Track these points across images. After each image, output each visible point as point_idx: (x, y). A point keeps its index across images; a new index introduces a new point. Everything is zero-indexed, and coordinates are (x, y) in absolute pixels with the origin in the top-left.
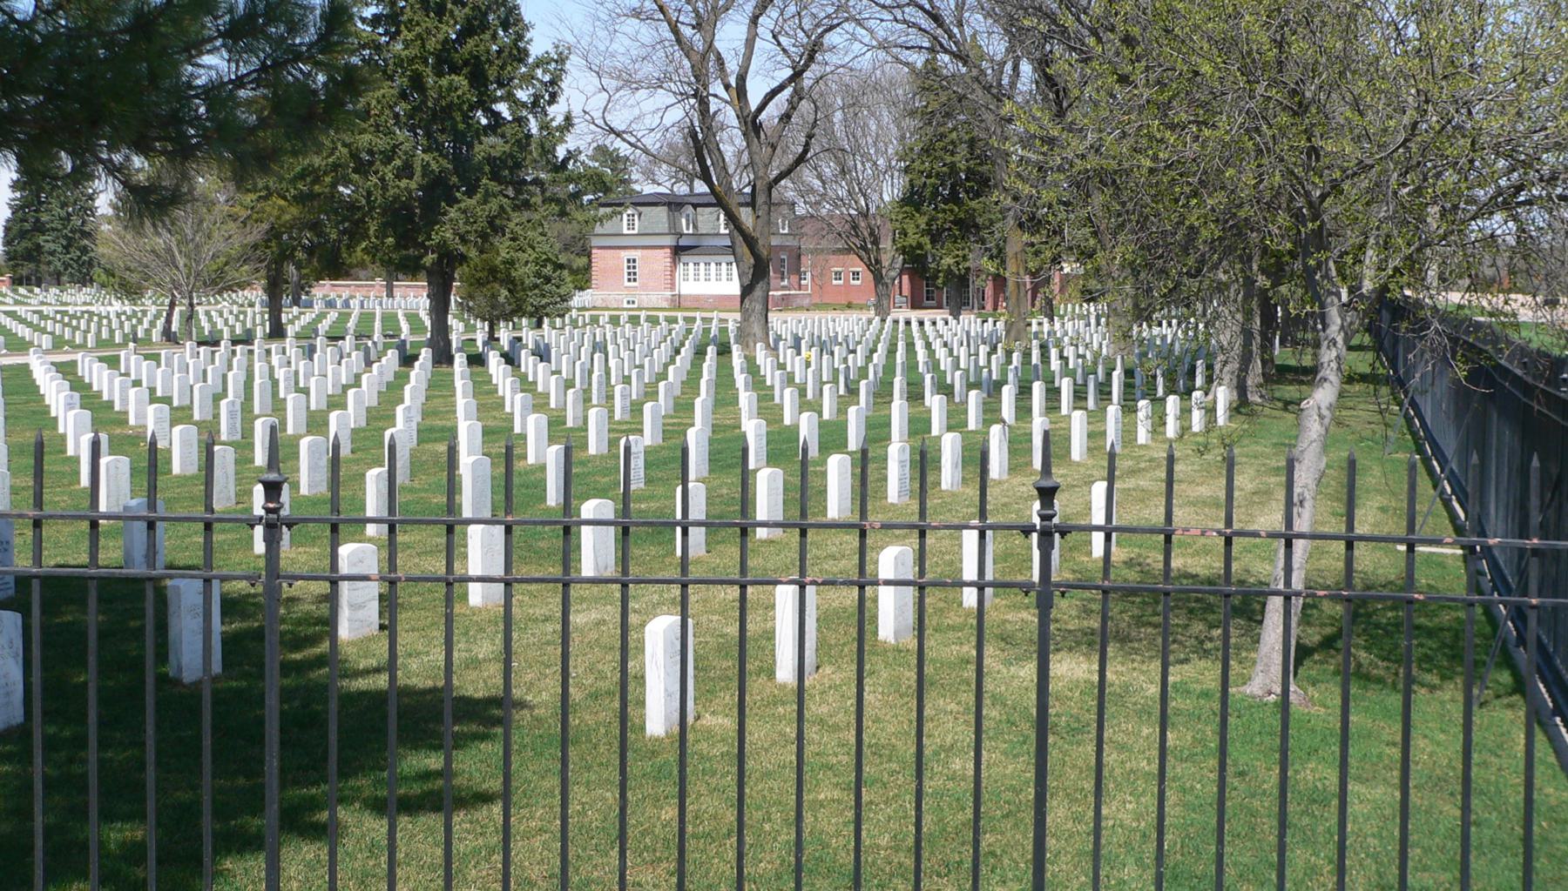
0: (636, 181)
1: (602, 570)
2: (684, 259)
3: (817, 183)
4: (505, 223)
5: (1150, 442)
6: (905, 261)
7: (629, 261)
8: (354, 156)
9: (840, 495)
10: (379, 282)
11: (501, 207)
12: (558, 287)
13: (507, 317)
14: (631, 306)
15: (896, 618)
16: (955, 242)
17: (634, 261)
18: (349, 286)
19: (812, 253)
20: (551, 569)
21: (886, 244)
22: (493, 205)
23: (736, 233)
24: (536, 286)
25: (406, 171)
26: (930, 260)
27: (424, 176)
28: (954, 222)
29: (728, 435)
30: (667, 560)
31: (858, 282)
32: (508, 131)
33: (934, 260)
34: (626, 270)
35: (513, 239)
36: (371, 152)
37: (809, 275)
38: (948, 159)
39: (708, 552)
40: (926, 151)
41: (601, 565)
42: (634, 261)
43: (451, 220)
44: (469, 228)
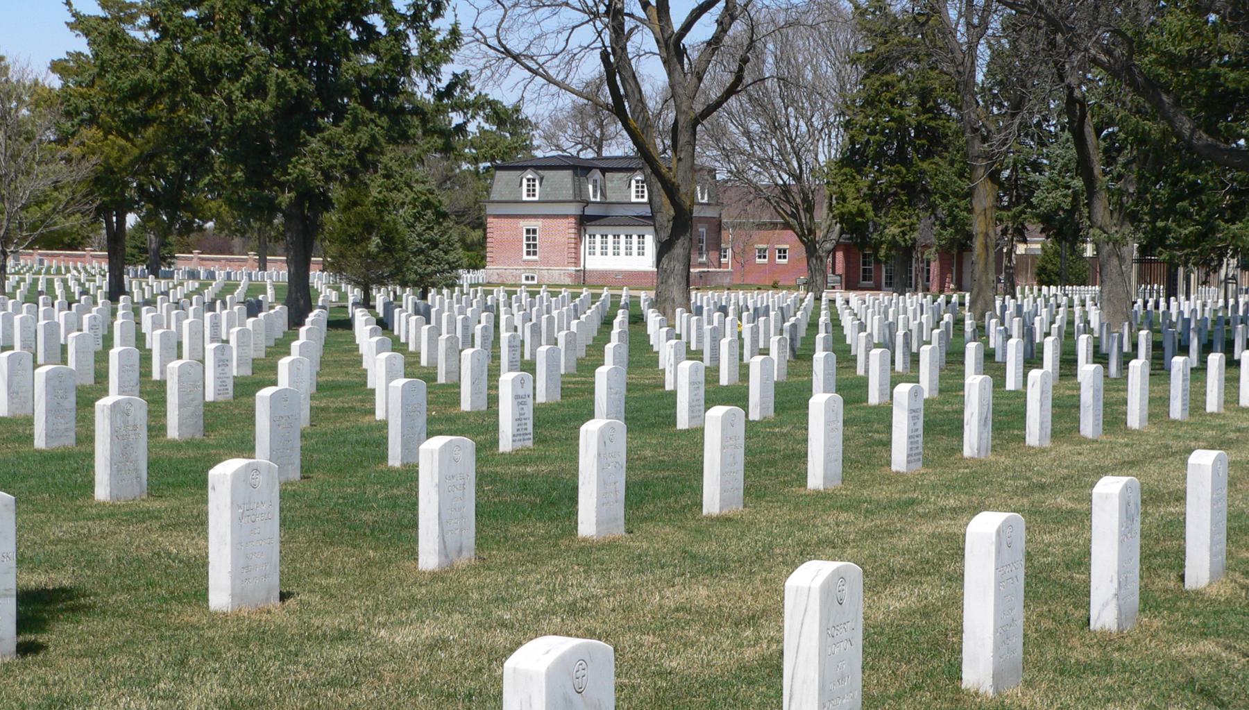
0: (538, 147)
1: (453, 555)
2: (590, 230)
3: (743, 143)
4: (377, 158)
5: (1222, 411)
6: (842, 232)
7: (528, 231)
8: (197, 71)
9: (827, 455)
10: (252, 256)
11: (373, 137)
12: (446, 253)
13: (381, 282)
14: (530, 282)
15: (997, 648)
16: (902, 209)
17: (534, 231)
18: (219, 260)
19: (734, 227)
20: (371, 553)
21: (822, 215)
22: (363, 136)
23: (654, 179)
24: (421, 251)
25: (258, 89)
26: (871, 229)
27: (279, 96)
28: (902, 186)
29: (649, 393)
30: (563, 543)
31: (785, 261)
32: (383, 47)
33: (875, 230)
34: (525, 242)
35: (387, 176)
36: (215, 66)
37: (729, 252)
38: (896, 112)
39: (629, 532)
40: (869, 102)
41: (452, 546)
42: (534, 231)
43: (313, 152)
44: (333, 161)
